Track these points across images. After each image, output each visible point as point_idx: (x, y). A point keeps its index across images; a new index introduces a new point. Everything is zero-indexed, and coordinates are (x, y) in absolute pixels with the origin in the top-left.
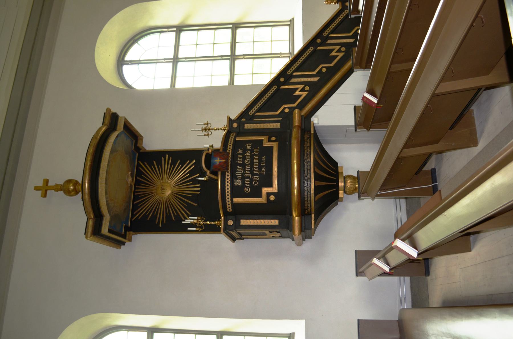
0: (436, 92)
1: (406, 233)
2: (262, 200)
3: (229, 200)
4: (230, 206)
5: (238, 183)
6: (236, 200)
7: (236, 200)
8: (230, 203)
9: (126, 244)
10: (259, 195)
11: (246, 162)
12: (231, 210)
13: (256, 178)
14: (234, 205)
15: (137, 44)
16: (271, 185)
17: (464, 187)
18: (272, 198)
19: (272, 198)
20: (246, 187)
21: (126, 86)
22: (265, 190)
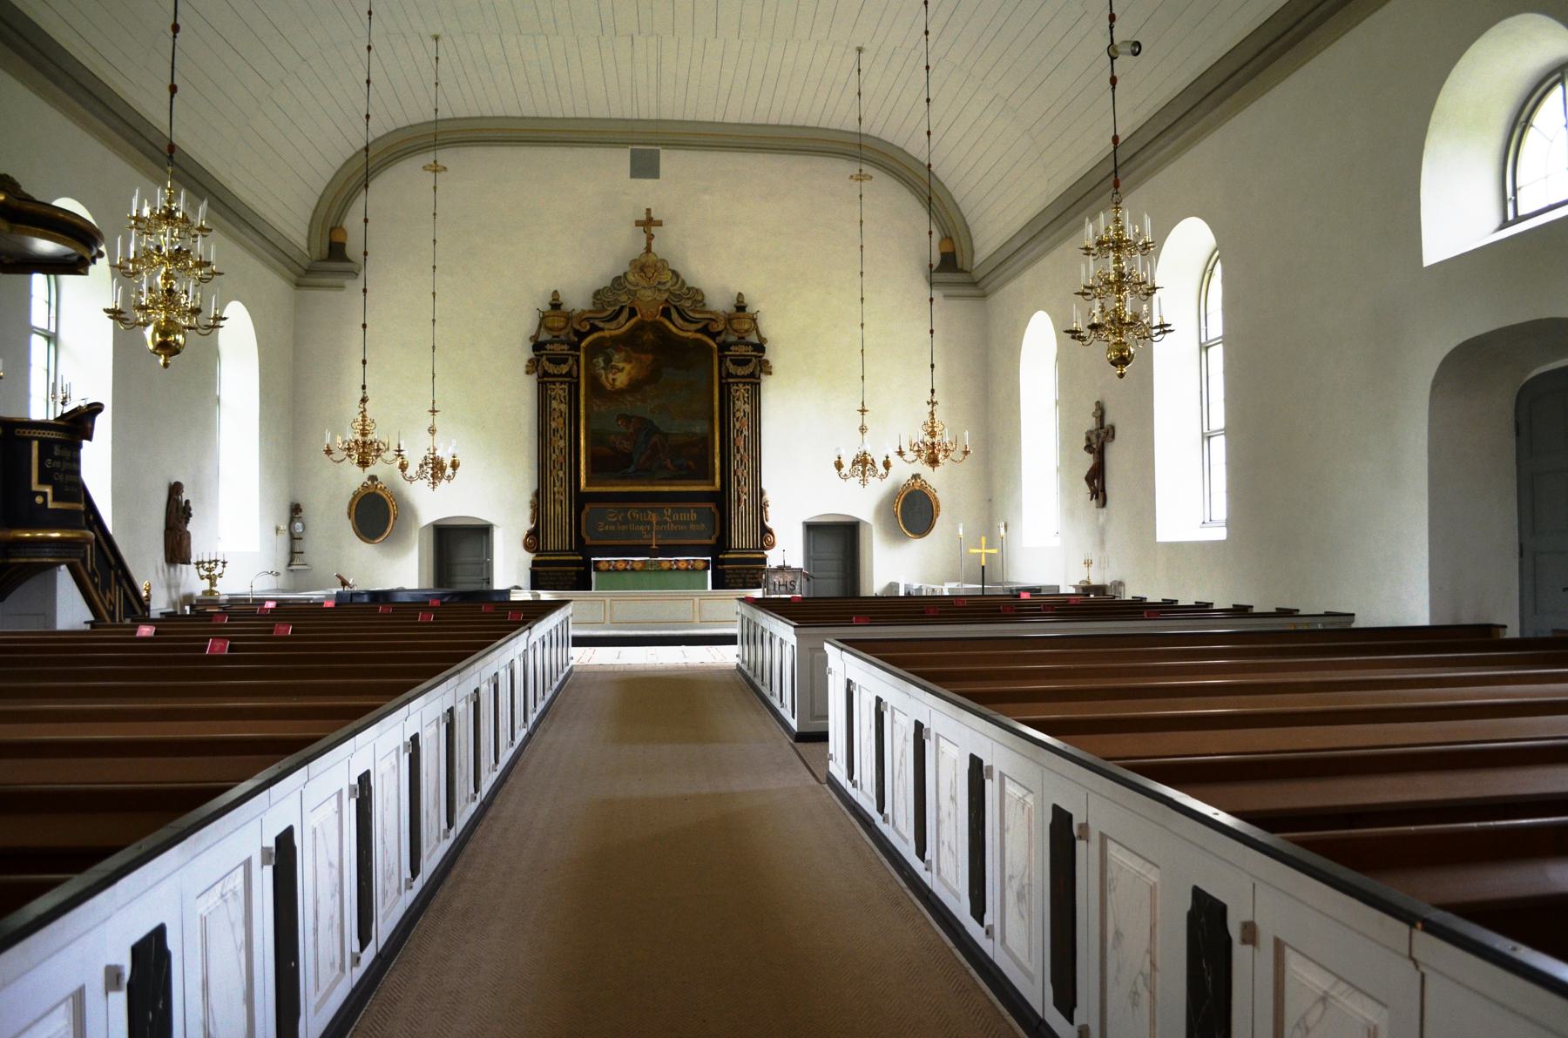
0: (1006, 778)
1: (841, 801)
2: (35, 487)
3: (36, 435)
4: (26, 434)
5: (57, 451)
6: (35, 444)
7: (35, 444)
8: (32, 434)
9: (664, 165)
10: (41, 481)
11: (634, 514)
12: (17, 434)
13: (61, 477)
14: (29, 440)
15: (45, 276)
16: (55, 499)
17: (48, 706)
18: (39, 500)
19: (39, 500)
20: (52, 462)
21: (249, 250)
22: (48, 490)
